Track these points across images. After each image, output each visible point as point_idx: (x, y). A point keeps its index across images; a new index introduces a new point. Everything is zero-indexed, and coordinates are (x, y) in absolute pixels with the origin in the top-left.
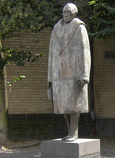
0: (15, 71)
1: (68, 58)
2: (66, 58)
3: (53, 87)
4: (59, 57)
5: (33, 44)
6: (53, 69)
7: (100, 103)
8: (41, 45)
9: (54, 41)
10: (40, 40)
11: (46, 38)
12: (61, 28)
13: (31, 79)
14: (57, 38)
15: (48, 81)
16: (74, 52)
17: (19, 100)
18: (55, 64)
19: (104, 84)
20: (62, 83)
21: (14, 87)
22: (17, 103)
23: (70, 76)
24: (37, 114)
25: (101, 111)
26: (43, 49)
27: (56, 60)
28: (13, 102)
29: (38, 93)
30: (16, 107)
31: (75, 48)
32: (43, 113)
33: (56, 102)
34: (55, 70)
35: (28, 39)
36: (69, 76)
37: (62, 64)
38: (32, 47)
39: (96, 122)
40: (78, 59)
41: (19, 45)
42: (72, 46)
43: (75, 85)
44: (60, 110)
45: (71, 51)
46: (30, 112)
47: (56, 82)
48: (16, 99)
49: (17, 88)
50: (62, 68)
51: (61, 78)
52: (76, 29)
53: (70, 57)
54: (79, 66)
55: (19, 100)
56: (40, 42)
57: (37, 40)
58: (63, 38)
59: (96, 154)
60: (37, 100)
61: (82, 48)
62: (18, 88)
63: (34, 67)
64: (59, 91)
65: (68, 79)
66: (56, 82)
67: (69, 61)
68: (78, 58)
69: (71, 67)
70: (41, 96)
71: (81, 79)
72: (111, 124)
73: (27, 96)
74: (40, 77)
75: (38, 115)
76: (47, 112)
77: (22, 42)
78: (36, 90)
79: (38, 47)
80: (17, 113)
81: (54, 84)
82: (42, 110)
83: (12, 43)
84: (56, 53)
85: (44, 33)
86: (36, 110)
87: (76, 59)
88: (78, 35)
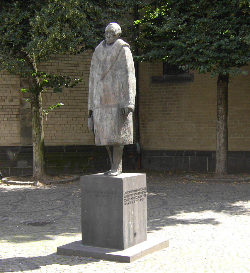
1: (110, 84)
2: (109, 83)
3: (94, 115)
4: (101, 83)
5: (72, 68)
6: (94, 95)
7: (146, 133)
8: (81, 69)
9: (96, 65)
10: (80, 64)
11: (86, 61)
12: (103, 50)
14: (99, 61)
15: (89, 109)
16: (117, 77)
17: (56, 131)
18: (96, 90)
20: (105, 111)
21: (51, 115)
22: (55, 133)
23: (113, 104)
24: (76, 146)
25: (148, 142)
27: (98, 85)
28: (49, 132)
29: (77, 123)
30: (53, 138)
31: (118, 72)
32: (83, 144)
33: (98, 132)
34: (97, 96)
35: (66, 62)
37: (104, 90)
38: (71, 71)
40: (121, 85)
41: (56, 69)
42: (115, 70)
43: (118, 113)
44: (102, 141)
45: (114, 76)
47: (97, 110)
48: (53, 128)
49: (53, 116)
51: (103, 106)
52: (120, 52)
53: (113, 82)
54: (123, 92)
55: (56, 131)
56: (80, 65)
57: (77, 63)
58: (105, 61)
59: (142, 190)
60: (77, 130)
61: (127, 72)
62: (56, 116)
63: (73, 93)
64: (101, 119)
65: (111, 107)
66: (97, 110)
67: (112, 86)
68: (122, 83)
69: (114, 93)
70: (81, 126)
71: (125, 106)
73: (66, 125)
74: (79, 104)
75: (77, 146)
76: (87, 144)
78: (76, 119)
79: (77, 72)
80: (54, 144)
81: (95, 112)
83: (48, 67)
84: (97, 78)
86: (75, 141)
87: (119, 85)
88: (121, 58)
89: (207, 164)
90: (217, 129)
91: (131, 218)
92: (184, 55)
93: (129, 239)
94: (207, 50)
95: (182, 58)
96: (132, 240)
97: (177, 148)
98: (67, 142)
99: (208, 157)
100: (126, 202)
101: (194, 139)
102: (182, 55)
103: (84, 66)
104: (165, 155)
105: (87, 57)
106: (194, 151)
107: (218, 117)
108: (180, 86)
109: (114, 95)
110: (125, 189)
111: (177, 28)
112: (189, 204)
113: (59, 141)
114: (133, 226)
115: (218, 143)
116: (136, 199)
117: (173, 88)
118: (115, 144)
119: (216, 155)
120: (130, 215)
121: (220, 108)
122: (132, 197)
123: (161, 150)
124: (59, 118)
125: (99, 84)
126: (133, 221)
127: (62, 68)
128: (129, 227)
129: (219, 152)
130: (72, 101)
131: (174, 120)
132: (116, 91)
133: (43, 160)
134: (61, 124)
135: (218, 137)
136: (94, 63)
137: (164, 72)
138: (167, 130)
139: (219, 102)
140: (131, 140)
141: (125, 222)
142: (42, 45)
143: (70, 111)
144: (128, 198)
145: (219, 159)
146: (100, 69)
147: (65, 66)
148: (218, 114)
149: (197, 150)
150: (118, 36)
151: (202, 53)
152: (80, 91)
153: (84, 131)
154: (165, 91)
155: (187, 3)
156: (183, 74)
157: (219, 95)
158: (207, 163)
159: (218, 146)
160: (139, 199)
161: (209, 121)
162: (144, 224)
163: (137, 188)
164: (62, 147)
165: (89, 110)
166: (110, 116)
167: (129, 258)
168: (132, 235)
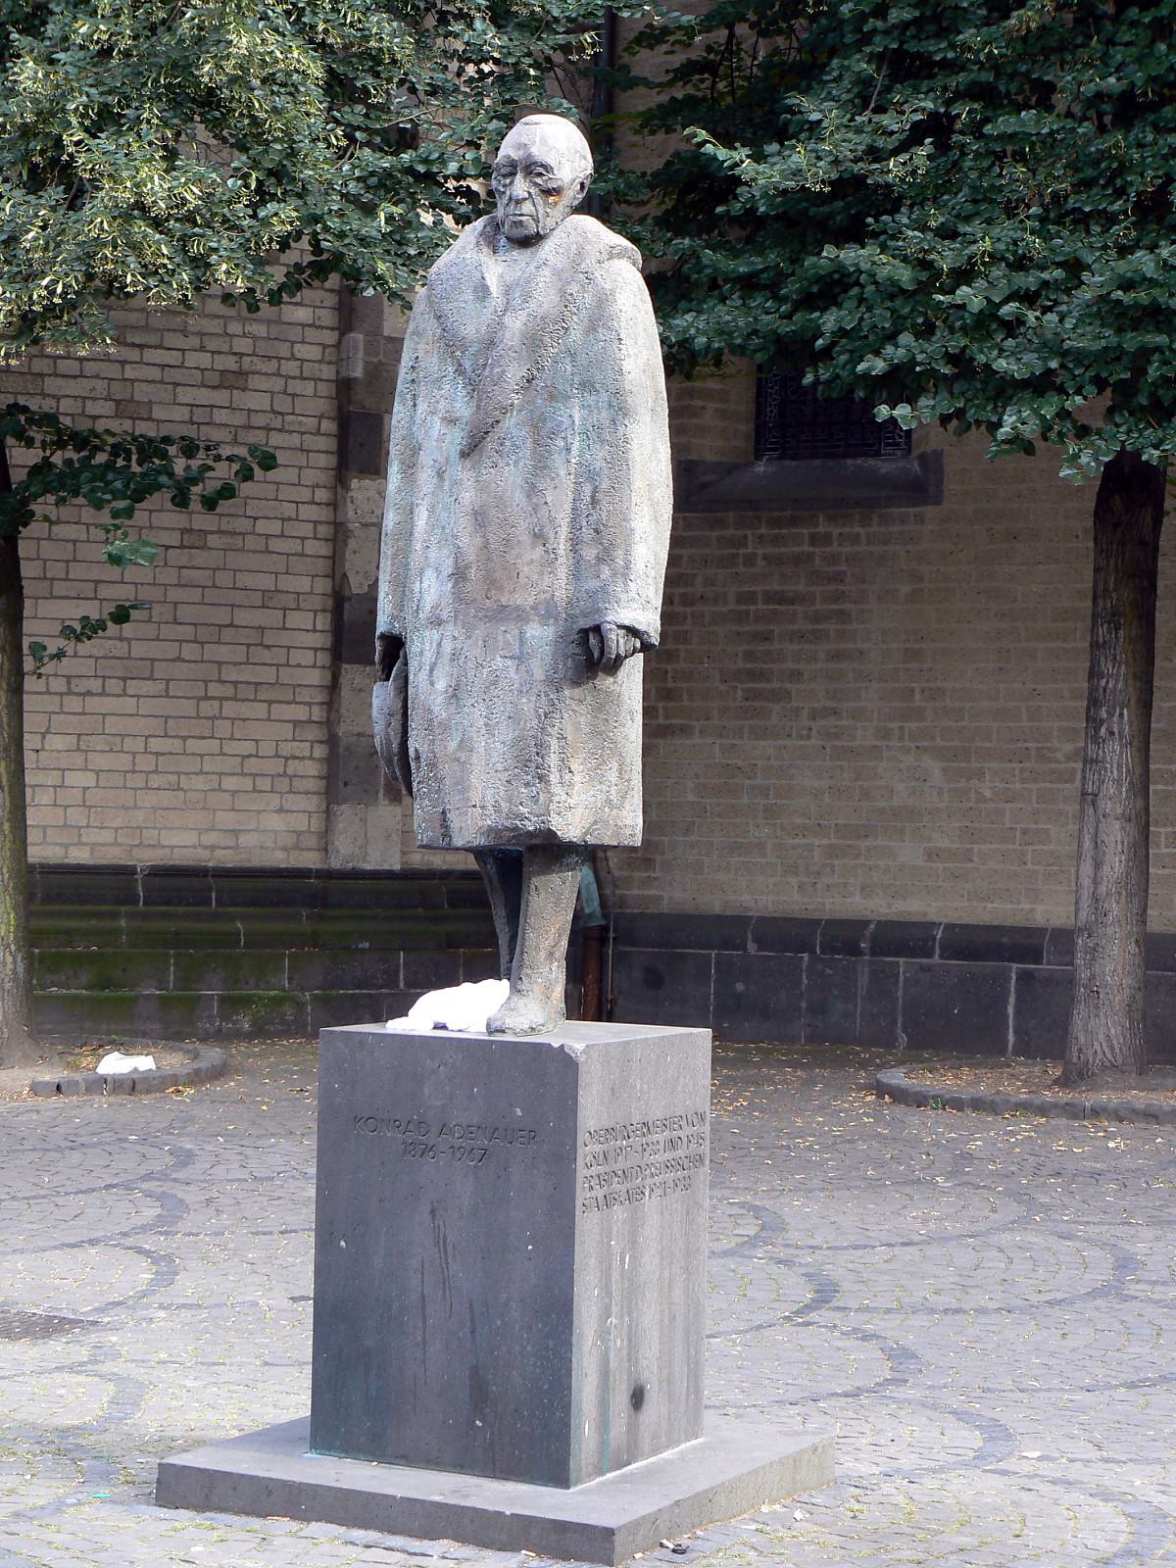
0: (76, 571)
1: (519, 481)
2: (509, 476)
4: (462, 472)
5: (204, 396)
6: (418, 546)
8: (259, 402)
9: (432, 363)
10: (253, 373)
11: (293, 358)
13: (186, 631)
14: (451, 343)
15: (382, 627)
17: (97, 772)
18: (427, 520)
19: (671, 685)
20: (480, 643)
21: (68, 678)
22: (85, 789)
23: (531, 600)
24: (215, 869)
26: (268, 429)
29: (223, 728)
30: (76, 817)
32: (257, 861)
33: (432, 766)
34: (433, 554)
35: (172, 358)
36: (525, 599)
37: (480, 518)
38: (200, 415)
39: (612, 935)
40: (587, 489)
44: (455, 821)
46: (167, 851)
47: (436, 635)
48: (78, 759)
49: (82, 686)
50: (478, 541)
53: (541, 465)
54: (597, 531)
55: (97, 772)
56: (255, 382)
57: (235, 367)
59: (683, 1123)
60: (221, 774)
61: (619, 409)
62: (95, 685)
63: (204, 547)
64: (455, 694)
65: (520, 616)
66: (432, 635)
67: (528, 496)
70: (248, 748)
72: (713, 953)
73: (155, 744)
74: (243, 617)
75: (222, 873)
76: (279, 859)
77: (133, 381)
78: (216, 703)
79: (239, 419)
80: (80, 856)
81: (422, 648)
82: (246, 840)
83: (60, 381)
84: (441, 439)
85: (279, 322)
86: (210, 839)
89: (1010, 1010)
90: (1084, 794)
91: (616, 1297)
92: (905, 338)
93: (603, 1425)
94: (1046, 310)
95: (896, 353)
96: (618, 1429)
97: (828, 907)
98: (159, 846)
99: (1015, 966)
100: (593, 1193)
101: (932, 855)
102: (892, 337)
103: (278, 384)
104: (752, 948)
105: (295, 333)
106: (934, 925)
107: (1093, 722)
108: (857, 529)
109: (540, 550)
110: (592, 1111)
111: (872, 172)
112: (917, 1238)
113: (107, 836)
114: (630, 1341)
115: (1086, 882)
116: (649, 1181)
117: (814, 539)
118: (534, 841)
119: (1070, 951)
120: (616, 1276)
121: (1107, 667)
122: (629, 1164)
123: (729, 913)
124: (118, 696)
125: (446, 476)
126: (630, 1313)
127: (141, 393)
128: (607, 1349)
129: (1089, 936)
130: (195, 595)
131: (814, 733)
132: (552, 520)
133: (18, 949)
134: (123, 736)
135: (1087, 844)
136: (421, 354)
137: (757, 442)
138: (767, 796)
139: (1102, 632)
140: (629, 822)
141: (585, 1314)
142: (52, 245)
143: (186, 655)
144: (607, 1169)
145: (1093, 977)
146: (461, 392)
147: (162, 382)
148: (1094, 702)
149: (945, 921)
150: (571, 193)
151: (1012, 327)
152: (249, 538)
153: (264, 784)
154: (765, 558)
155: (941, 22)
156: (877, 454)
157: (1106, 583)
158: (1012, 1000)
159: (1085, 895)
160: (670, 1176)
161: (1032, 745)
162: (687, 1332)
163: (657, 1113)
164: (127, 872)
165: (383, 636)
166: (512, 674)
167: (609, 1533)
168: (621, 1399)
